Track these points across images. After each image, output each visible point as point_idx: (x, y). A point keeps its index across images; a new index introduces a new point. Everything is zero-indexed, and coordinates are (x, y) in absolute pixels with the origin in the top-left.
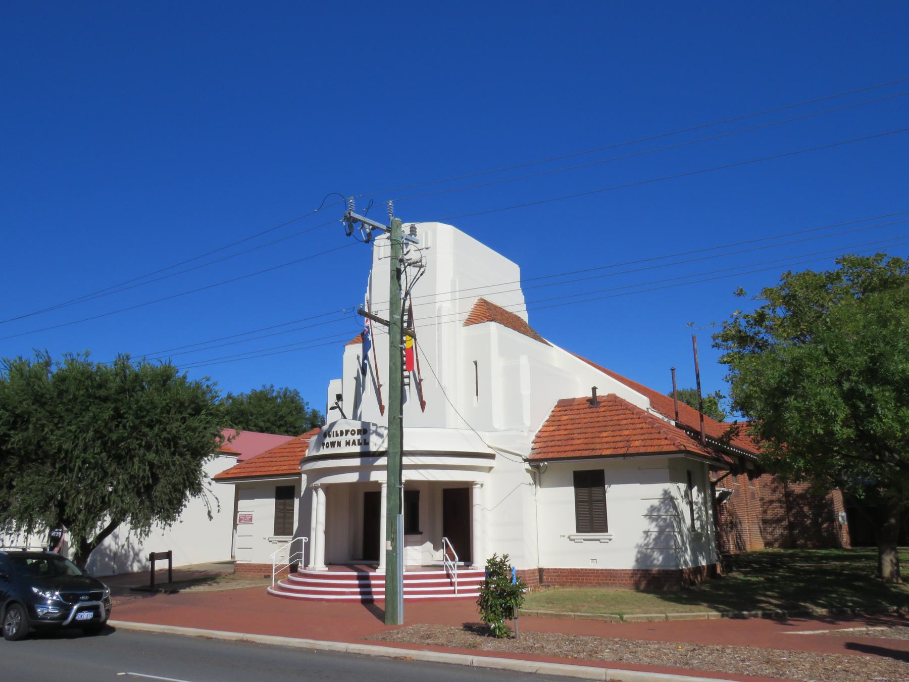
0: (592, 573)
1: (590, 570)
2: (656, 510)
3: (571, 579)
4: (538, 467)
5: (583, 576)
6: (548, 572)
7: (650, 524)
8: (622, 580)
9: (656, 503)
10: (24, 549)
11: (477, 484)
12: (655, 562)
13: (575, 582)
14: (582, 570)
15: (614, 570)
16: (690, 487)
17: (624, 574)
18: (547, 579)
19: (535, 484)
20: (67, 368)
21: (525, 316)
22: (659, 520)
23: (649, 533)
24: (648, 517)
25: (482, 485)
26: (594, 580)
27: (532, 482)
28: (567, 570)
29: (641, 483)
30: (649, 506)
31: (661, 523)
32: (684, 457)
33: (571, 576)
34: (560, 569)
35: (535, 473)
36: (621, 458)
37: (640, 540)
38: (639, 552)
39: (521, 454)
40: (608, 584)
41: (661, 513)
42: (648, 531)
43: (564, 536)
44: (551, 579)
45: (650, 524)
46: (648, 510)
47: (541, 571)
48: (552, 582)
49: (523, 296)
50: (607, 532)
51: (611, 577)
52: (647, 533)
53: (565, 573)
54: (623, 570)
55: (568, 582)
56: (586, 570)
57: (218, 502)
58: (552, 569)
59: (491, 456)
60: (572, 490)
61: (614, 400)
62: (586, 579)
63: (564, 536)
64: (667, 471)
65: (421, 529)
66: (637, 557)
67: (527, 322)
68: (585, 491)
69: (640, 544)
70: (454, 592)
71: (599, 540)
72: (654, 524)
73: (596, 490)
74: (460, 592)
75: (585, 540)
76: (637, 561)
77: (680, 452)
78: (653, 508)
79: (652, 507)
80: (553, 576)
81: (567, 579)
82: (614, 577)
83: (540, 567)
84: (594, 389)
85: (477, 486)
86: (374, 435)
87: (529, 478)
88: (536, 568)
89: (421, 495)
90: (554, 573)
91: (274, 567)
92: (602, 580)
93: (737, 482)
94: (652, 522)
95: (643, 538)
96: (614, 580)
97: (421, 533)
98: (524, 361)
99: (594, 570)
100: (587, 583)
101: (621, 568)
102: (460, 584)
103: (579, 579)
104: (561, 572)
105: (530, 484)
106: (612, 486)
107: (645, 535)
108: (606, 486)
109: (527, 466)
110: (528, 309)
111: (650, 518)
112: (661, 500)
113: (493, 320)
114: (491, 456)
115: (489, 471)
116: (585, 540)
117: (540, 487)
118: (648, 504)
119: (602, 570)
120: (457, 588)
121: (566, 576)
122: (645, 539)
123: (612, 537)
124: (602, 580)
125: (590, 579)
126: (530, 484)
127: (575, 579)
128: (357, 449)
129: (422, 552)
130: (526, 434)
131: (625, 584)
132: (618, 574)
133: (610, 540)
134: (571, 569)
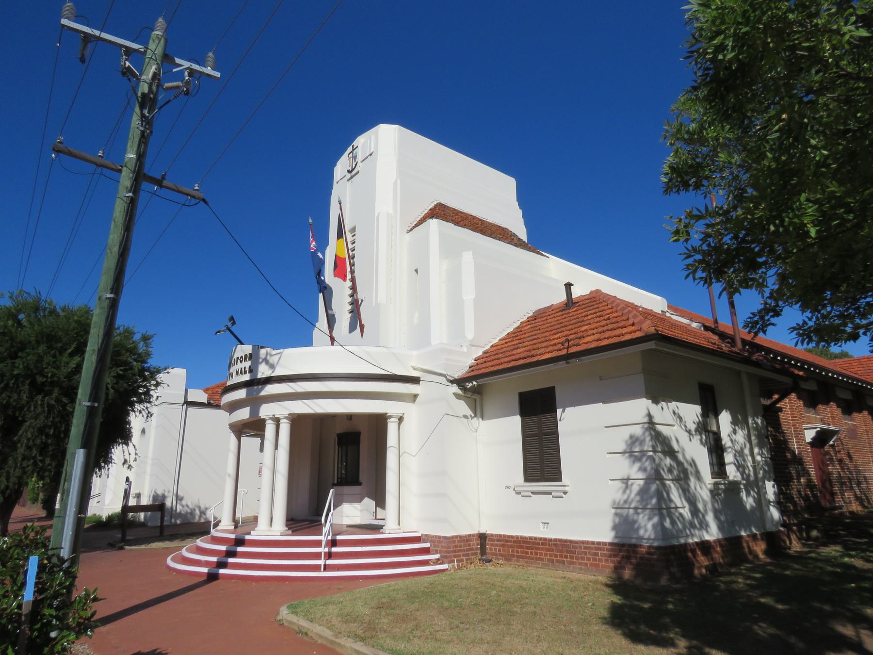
0: (543, 544)
1: (541, 539)
2: (637, 443)
3: (517, 552)
4: (477, 391)
5: (531, 548)
6: (493, 540)
7: (631, 467)
8: (582, 559)
9: (638, 431)
10: (19, 502)
11: (391, 417)
12: (642, 532)
13: (523, 557)
14: (531, 538)
15: (571, 542)
16: (710, 409)
17: (586, 548)
18: (491, 549)
19: (476, 416)
20: (134, 339)
21: (522, 233)
22: (644, 459)
23: (630, 482)
24: (627, 455)
25: (401, 419)
26: (546, 555)
27: (469, 412)
28: (513, 537)
29: (604, 402)
30: (627, 437)
31: (647, 464)
32: (654, 347)
33: (518, 547)
34: (505, 536)
35: (475, 399)
36: (562, 364)
37: (614, 493)
38: (616, 514)
39: (445, 373)
40: (563, 562)
41: (646, 448)
42: (628, 479)
43: (509, 487)
44: (495, 550)
45: (631, 467)
46: (626, 442)
47: (483, 537)
48: (496, 554)
49: (521, 210)
50: (561, 481)
51: (567, 551)
52: (626, 481)
53: (511, 541)
54: (583, 542)
55: (514, 556)
56: (536, 538)
57: (136, 450)
58: (496, 535)
59: (415, 380)
60: (517, 420)
61: (596, 299)
62: (536, 554)
63: (509, 487)
64: (642, 375)
65: (361, 479)
66: (614, 522)
67: (175, 58)
68: (533, 419)
69: (617, 501)
70: (316, 568)
71: (549, 493)
72: (637, 465)
73: (545, 418)
74: (326, 568)
75: (533, 493)
76: (615, 528)
77: (647, 338)
78: (634, 440)
79: (631, 437)
80: (497, 545)
81: (513, 551)
82: (573, 552)
83: (481, 532)
84: (568, 286)
85: (392, 419)
86: (264, 363)
87: (463, 407)
88: (477, 532)
89: (362, 436)
90: (498, 540)
91: (212, 523)
92: (556, 556)
93: (852, 420)
94: (634, 462)
95: (621, 491)
96: (572, 558)
97: (360, 484)
98: (468, 257)
99: (545, 539)
100: (537, 559)
101: (581, 539)
102: (317, 556)
103: (527, 553)
104: (506, 541)
105: (465, 417)
106: (567, 409)
107: (624, 485)
108: (559, 411)
109: (455, 389)
110: (526, 224)
111: (630, 456)
112: (646, 426)
113: (433, 217)
114: (415, 380)
115: (414, 401)
116: (533, 493)
117: (483, 420)
118: (625, 434)
119: (556, 540)
120: (321, 562)
121: (512, 547)
122: (624, 492)
123: (566, 489)
124: (556, 556)
125: (541, 554)
126: (465, 417)
127: (522, 552)
128: (246, 377)
129: (361, 511)
130: (465, 350)
131: (586, 564)
132: (575, 547)
133: (565, 493)
134: (517, 537)
